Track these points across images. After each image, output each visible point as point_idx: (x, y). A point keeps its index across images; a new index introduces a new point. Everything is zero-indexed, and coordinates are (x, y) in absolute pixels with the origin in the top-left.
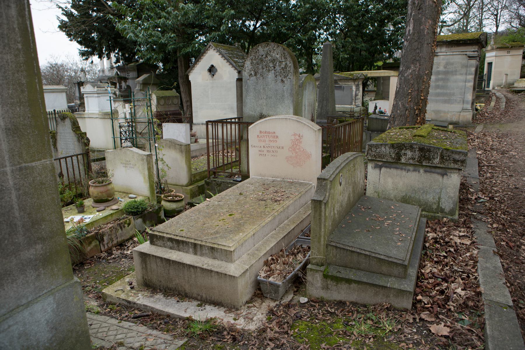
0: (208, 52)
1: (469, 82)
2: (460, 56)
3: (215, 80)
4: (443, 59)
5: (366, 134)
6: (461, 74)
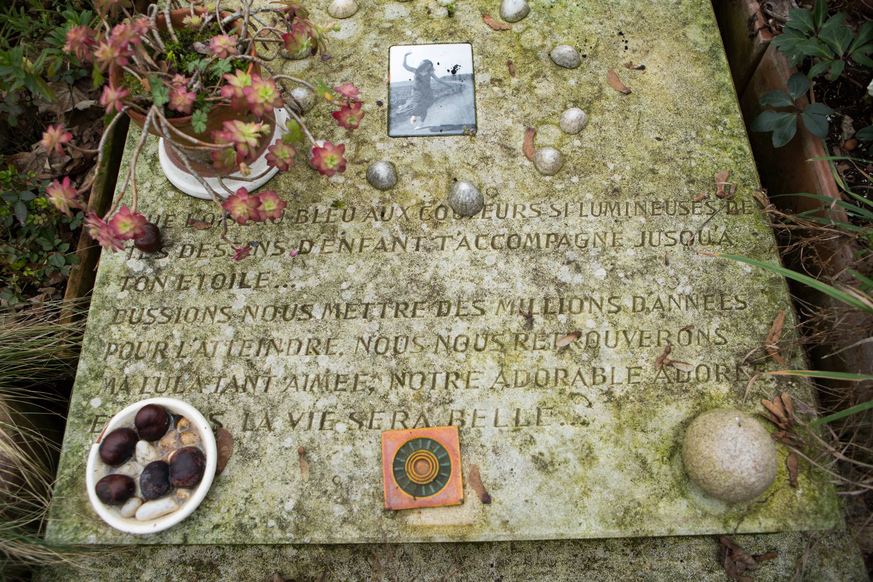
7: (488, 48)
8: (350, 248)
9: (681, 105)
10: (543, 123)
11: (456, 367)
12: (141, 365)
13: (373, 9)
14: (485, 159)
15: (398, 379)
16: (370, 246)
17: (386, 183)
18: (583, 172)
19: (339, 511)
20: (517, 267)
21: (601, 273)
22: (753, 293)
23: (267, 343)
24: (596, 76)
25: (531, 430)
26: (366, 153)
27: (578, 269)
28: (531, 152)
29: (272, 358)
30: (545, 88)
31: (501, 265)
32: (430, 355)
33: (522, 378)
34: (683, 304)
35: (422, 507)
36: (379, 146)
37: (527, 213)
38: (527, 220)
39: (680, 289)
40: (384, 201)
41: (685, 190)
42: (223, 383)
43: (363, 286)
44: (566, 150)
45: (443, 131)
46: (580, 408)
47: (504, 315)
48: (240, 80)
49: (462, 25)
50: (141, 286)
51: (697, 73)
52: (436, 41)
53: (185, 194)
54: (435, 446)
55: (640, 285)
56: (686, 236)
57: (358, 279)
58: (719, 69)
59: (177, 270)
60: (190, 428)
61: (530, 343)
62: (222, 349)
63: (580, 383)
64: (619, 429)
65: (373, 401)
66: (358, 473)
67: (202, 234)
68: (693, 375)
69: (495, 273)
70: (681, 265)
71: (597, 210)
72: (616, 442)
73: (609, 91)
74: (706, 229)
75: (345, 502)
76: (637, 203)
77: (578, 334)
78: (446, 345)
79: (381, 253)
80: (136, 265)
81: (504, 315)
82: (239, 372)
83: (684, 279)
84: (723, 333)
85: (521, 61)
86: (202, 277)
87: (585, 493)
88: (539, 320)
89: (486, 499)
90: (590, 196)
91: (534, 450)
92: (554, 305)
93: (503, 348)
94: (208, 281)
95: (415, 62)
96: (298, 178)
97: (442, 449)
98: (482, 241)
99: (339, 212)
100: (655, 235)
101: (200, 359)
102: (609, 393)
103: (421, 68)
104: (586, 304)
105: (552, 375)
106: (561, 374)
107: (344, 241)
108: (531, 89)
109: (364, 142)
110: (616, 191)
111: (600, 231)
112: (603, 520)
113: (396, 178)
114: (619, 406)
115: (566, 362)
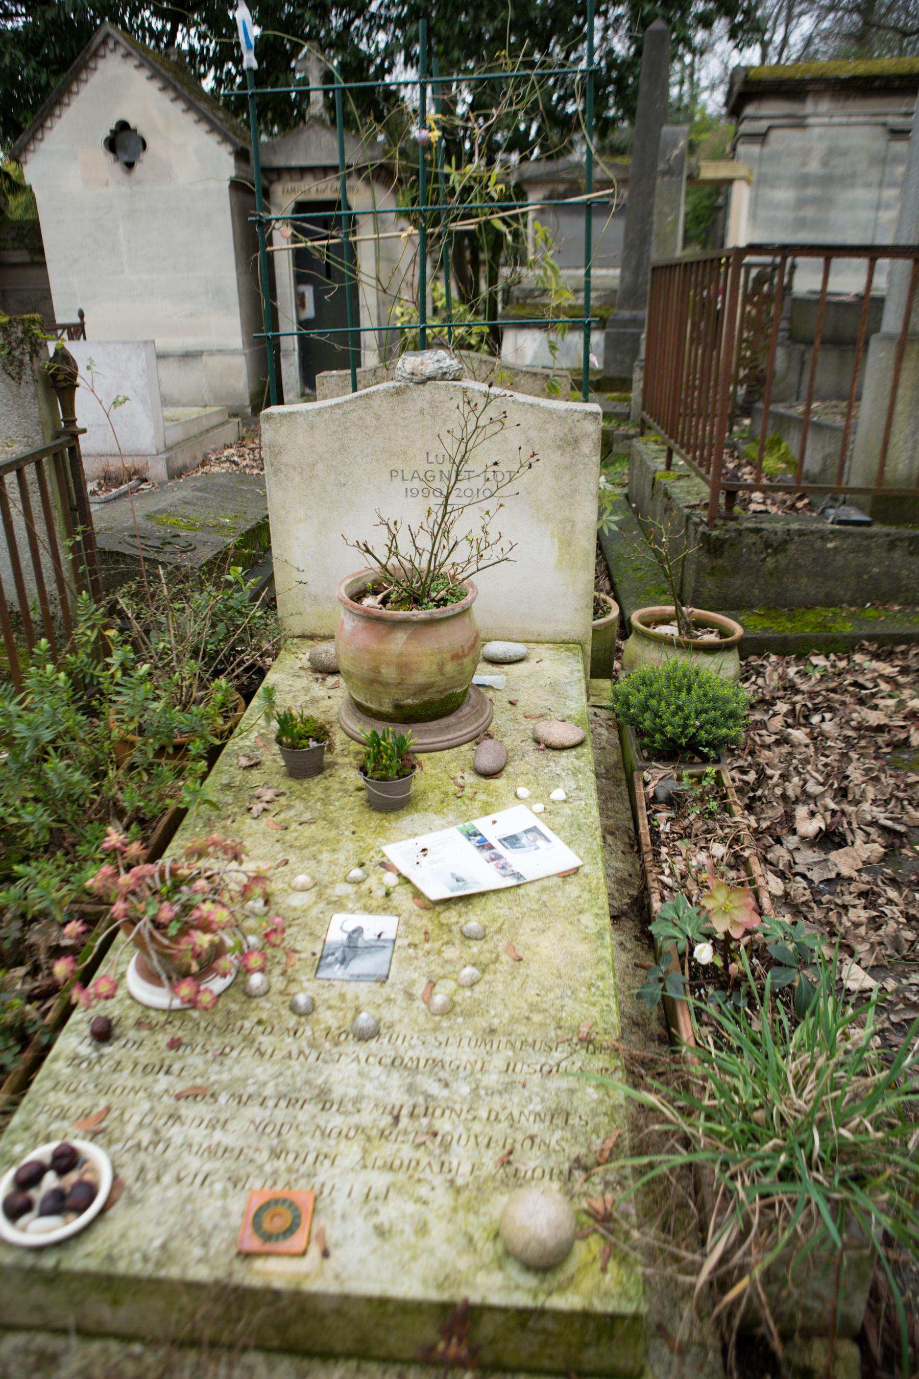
0: (101, 64)
1: (888, 207)
2: (866, 130)
3: (139, 182)
4: (821, 138)
5: (789, 355)
6: (868, 185)
7: (412, 921)
8: (262, 1055)
9: (563, 971)
10: (444, 977)
11: (325, 1150)
12: (66, 1124)
13: (326, 887)
14: (389, 1000)
15: (275, 1154)
16: (278, 1055)
17: (303, 1009)
18: (468, 1014)
19: (197, 1252)
20: (396, 1080)
21: (465, 1089)
22: (594, 1113)
23: (174, 1117)
24: (496, 946)
25: (379, 1205)
26: (293, 988)
27: (447, 1085)
28: (427, 998)
29: (176, 1129)
30: (450, 953)
31: (383, 1078)
32: (307, 1139)
33: (379, 1163)
34: (532, 1118)
35: (268, 1254)
36: (306, 984)
37: (413, 1042)
38: (412, 1047)
39: (531, 1107)
40: (299, 1023)
41: (553, 1034)
42: (129, 1144)
43: (265, 1084)
44: (457, 998)
45: (358, 978)
46: (423, 1191)
47: (376, 1114)
48: (207, 907)
49: (395, 903)
50: (84, 1065)
51: (583, 949)
52: (371, 912)
53: (139, 1003)
54: (291, 1205)
55: (497, 1102)
56: (546, 1068)
57: (263, 1077)
58: (603, 946)
59: (117, 1057)
60: (94, 1170)
61: (393, 1137)
62: (137, 1119)
63: (428, 1170)
64: (455, 1210)
65: (250, 1168)
66: (223, 1223)
67: (145, 1033)
68: (529, 1174)
69: (376, 1083)
70: (536, 1089)
71: (473, 1043)
72: (450, 1221)
73: (504, 958)
74: (563, 1064)
75: (205, 1245)
76: (508, 1042)
77: (435, 1134)
78: (323, 1133)
79: (288, 1062)
80: (85, 1049)
81: (376, 1114)
82: (145, 1137)
83: (536, 1100)
84: (563, 1143)
85: (436, 931)
86: (136, 1065)
87: (414, 1258)
88: (404, 1121)
89: (326, 1254)
90: (469, 1033)
91: (377, 1220)
92: (420, 1110)
93: (369, 1139)
94: (140, 1068)
95: (350, 928)
96: (235, 1001)
97: (297, 1209)
98: (371, 1060)
99: (261, 1028)
100: (519, 1066)
101: (116, 1124)
102: (452, 1182)
103: (354, 932)
104: (447, 1113)
105: (406, 1163)
106: (413, 1164)
107: (258, 1050)
108: (440, 952)
109: (294, 980)
110: (493, 1031)
111: (472, 1059)
112: (424, 1282)
113: (312, 1007)
114: (458, 1191)
115: (420, 1154)
